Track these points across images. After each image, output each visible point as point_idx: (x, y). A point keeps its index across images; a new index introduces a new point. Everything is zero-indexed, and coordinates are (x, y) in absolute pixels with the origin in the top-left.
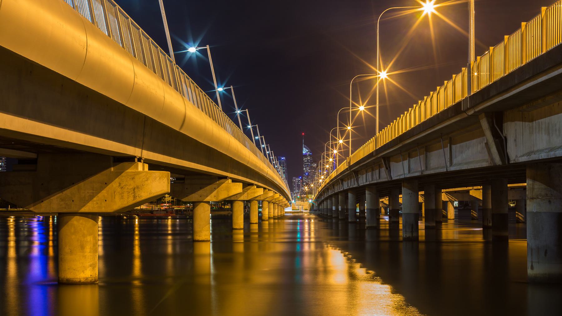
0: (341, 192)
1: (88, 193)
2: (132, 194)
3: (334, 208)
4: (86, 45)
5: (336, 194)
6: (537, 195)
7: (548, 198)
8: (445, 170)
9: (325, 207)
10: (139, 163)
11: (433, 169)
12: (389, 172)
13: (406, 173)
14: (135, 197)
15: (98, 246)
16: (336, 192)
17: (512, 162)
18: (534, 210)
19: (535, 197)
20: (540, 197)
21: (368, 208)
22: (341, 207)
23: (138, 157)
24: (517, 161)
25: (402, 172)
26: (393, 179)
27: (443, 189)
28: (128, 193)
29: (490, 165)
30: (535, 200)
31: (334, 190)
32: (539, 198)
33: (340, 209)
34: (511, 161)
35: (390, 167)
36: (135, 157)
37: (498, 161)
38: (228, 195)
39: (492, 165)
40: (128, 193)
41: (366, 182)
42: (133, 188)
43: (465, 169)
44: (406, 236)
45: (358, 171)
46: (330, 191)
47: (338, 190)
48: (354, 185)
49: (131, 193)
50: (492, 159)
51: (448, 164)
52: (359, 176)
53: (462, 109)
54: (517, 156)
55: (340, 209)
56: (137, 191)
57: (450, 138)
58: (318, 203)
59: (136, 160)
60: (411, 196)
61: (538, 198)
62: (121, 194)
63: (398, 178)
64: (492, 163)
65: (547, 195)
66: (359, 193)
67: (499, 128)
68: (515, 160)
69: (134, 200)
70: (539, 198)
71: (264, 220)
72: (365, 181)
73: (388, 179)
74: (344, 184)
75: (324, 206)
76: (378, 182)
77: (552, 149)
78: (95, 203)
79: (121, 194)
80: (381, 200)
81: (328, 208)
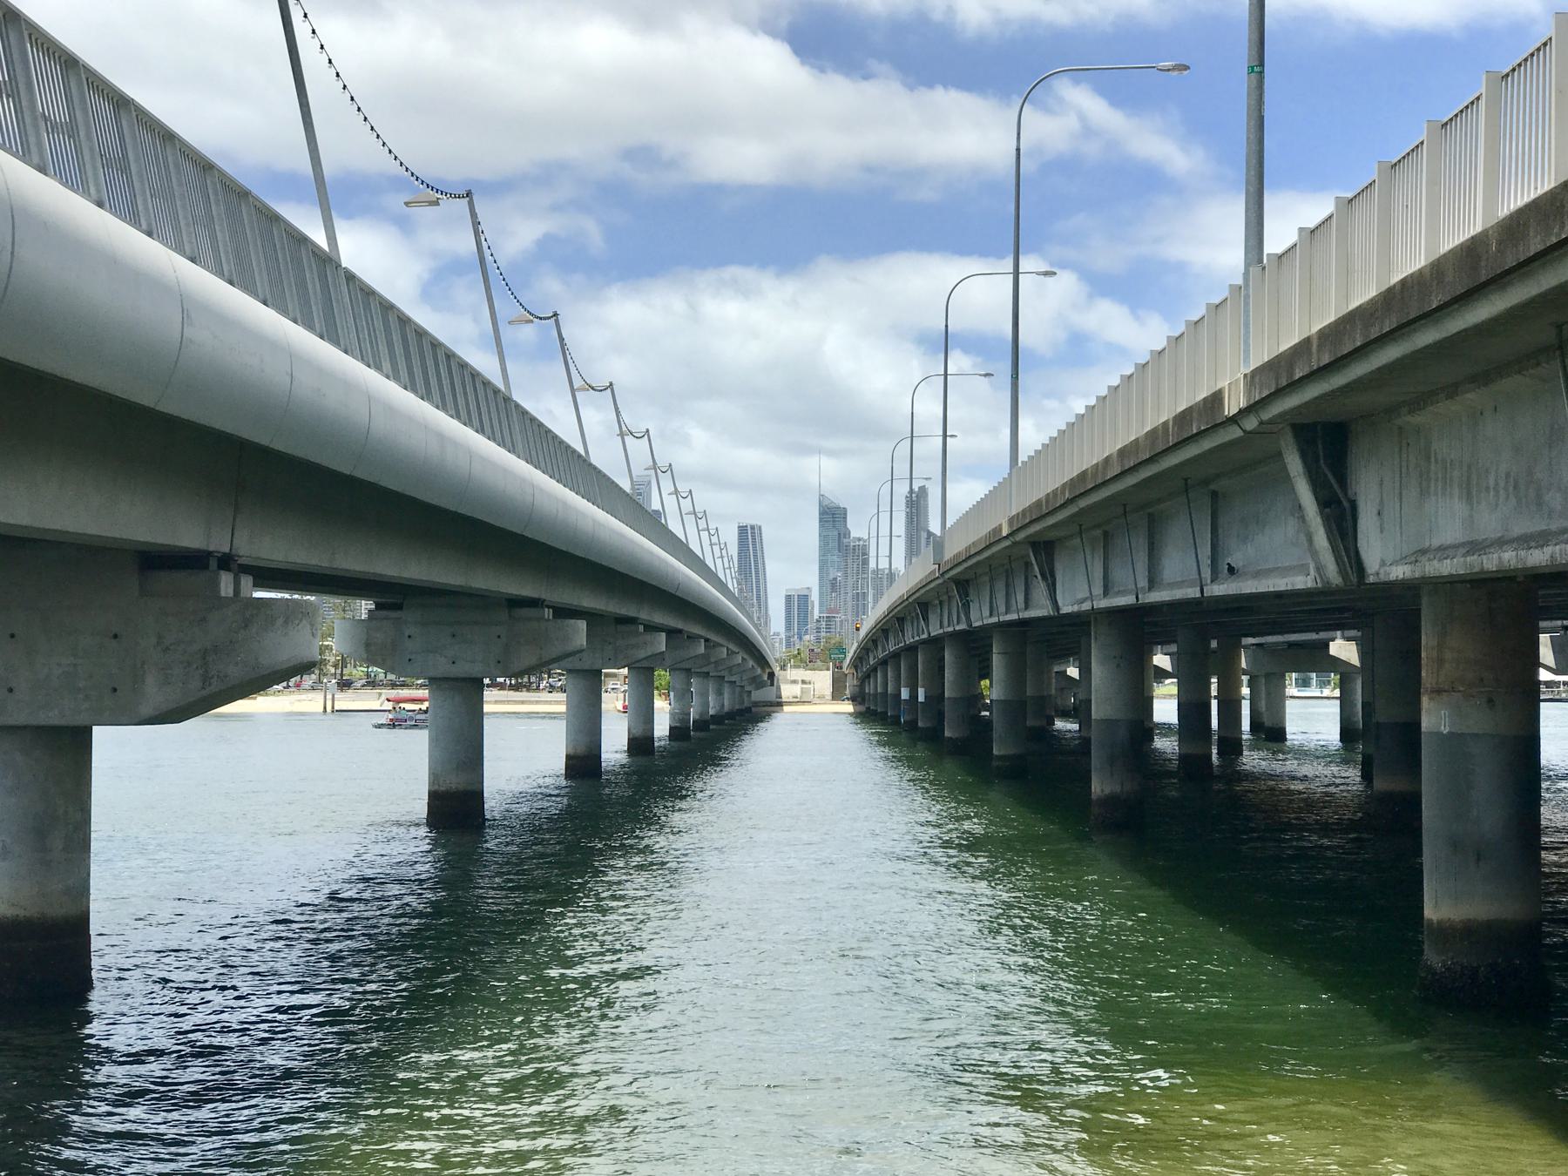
0: (924, 642)
1: (59, 665)
2: (197, 668)
3: (905, 694)
4: (11, 240)
5: (912, 649)
6: (1453, 682)
7: (1483, 690)
8: (1193, 593)
9: (872, 692)
10: (222, 572)
11: (1172, 585)
12: (1050, 591)
13: (1097, 596)
14: (206, 679)
15: (1261, 423)
16: (907, 643)
17: (1371, 579)
18: (1443, 727)
19: (1446, 688)
20: (1461, 689)
21: (1002, 698)
22: (925, 692)
23: (219, 555)
24: (1383, 578)
25: (1084, 594)
26: (1061, 612)
27: (1247, 636)
28: (185, 668)
29: (1315, 586)
30: (1445, 696)
31: (903, 635)
32: (1459, 691)
33: (921, 698)
34: (1368, 577)
35: (928, 618)
36: (210, 554)
37: (1334, 577)
38: (541, 658)
39: (1320, 585)
40: (185, 668)
41: (991, 615)
42: (200, 650)
43: (1249, 592)
44: (1102, 791)
45: (967, 581)
46: (934, 619)
47: (941, 627)
48: (958, 623)
49: (195, 666)
50: (1320, 569)
51: (1207, 573)
52: (971, 592)
53: (1226, 413)
54: (1383, 564)
55: (921, 698)
56: (213, 660)
57: (1150, 515)
58: (860, 675)
59: (213, 564)
60: (1118, 666)
61: (1454, 691)
62: (163, 669)
63: (1076, 608)
64: (1318, 581)
65: (1482, 680)
66: (974, 646)
67: (1334, 475)
68: (1378, 574)
69: (203, 688)
70: (1459, 691)
71: (1093, 607)
72: (986, 613)
73: (1048, 612)
74: (930, 621)
75: (875, 686)
76: (985, 623)
77: (1474, 547)
78: (81, 696)
79: (163, 669)
80: (1056, 669)
81: (889, 692)
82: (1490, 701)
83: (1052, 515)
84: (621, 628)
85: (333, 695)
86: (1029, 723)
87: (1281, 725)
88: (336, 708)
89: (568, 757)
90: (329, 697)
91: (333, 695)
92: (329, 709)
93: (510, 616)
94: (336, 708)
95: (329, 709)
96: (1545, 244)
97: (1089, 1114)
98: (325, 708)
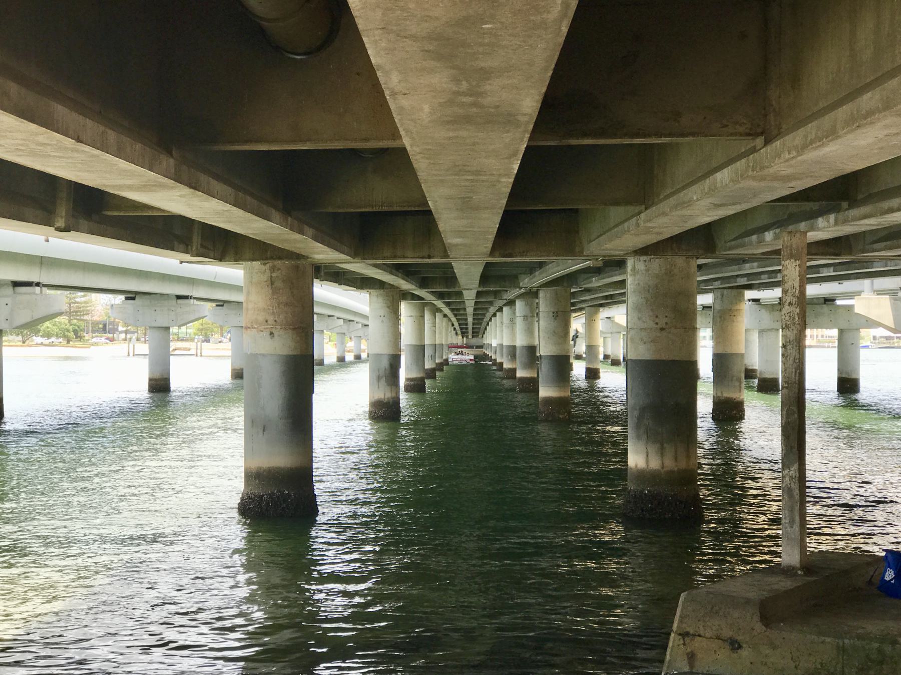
20: (256, 327)
38: (32, 318)
60: (382, 321)
82: (272, 333)
83: (828, 267)
84: (180, 301)
85: (134, 346)
86: (437, 362)
87: (854, 376)
88: (135, 353)
89: (150, 380)
90: (131, 346)
91: (134, 346)
92: (131, 354)
93: (14, 293)
94: (135, 353)
95: (131, 354)
96: (509, 120)
97: (325, 648)
98: (129, 353)
